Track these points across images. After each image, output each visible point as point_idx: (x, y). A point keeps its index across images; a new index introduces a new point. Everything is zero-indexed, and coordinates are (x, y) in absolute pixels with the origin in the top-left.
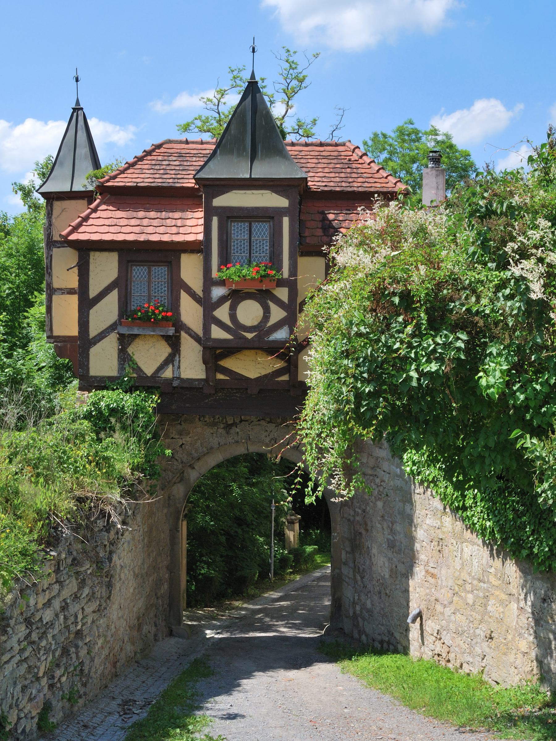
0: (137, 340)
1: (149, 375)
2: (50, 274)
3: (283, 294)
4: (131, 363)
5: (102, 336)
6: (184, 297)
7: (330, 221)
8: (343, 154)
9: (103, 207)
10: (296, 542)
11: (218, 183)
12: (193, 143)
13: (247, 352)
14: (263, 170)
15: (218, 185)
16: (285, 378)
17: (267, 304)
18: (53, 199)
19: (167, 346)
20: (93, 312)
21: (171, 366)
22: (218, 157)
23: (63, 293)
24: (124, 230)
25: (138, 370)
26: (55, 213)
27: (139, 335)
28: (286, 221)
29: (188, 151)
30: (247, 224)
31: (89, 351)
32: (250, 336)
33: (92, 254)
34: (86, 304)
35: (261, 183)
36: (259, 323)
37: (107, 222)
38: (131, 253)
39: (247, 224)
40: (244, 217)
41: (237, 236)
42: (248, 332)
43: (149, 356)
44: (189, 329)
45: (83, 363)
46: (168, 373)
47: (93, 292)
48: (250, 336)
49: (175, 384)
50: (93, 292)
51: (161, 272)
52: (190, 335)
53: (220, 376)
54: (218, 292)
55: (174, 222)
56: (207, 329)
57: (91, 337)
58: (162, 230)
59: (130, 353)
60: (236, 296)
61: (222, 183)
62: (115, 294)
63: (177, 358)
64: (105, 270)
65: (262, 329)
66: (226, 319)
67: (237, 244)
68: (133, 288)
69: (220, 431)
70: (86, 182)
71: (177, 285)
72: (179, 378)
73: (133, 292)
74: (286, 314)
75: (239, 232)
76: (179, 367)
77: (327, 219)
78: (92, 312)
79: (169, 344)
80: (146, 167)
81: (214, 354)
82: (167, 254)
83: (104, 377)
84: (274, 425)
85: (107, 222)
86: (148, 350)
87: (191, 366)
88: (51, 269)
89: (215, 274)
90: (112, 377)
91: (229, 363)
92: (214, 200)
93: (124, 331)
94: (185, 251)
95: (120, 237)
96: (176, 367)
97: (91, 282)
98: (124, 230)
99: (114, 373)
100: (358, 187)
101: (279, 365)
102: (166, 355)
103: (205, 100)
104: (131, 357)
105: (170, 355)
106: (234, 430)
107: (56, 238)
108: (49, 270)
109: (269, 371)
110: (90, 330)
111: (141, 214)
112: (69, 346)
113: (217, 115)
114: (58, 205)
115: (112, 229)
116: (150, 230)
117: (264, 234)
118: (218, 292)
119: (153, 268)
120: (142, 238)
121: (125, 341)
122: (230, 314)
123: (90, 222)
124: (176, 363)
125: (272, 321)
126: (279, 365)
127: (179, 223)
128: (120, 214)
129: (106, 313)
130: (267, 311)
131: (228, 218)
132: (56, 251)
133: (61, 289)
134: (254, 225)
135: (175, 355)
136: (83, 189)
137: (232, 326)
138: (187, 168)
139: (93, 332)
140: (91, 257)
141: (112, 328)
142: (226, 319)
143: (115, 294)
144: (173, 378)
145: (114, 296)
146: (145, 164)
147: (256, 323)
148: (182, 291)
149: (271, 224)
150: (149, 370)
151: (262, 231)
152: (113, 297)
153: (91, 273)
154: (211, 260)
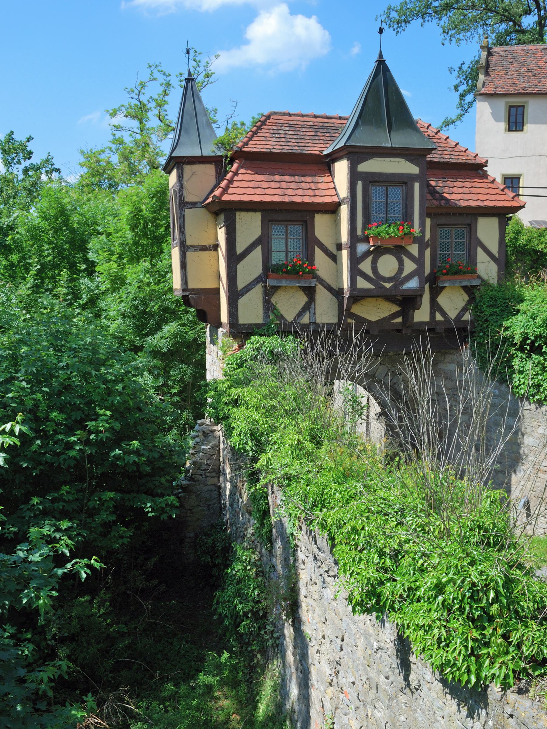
3: (414, 249)
4: (275, 311)
5: (248, 288)
6: (318, 253)
7: (434, 187)
9: (242, 171)
11: (363, 150)
12: (295, 115)
13: (370, 299)
15: (356, 153)
16: (400, 320)
17: (402, 258)
18: (184, 163)
21: (308, 313)
22: (361, 128)
23: (195, 250)
25: (281, 317)
26: (186, 176)
27: (281, 286)
28: (417, 185)
30: (384, 188)
31: (237, 301)
32: (388, 285)
33: (238, 214)
37: (252, 184)
38: (272, 213)
42: (387, 282)
44: (322, 280)
46: (306, 319)
47: (240, 249)
48: (388, 285)
50: (240, 249)
51: (296, 229)
52: (323, 286)
54: (362, 248)
55: (308, 186)
57: (239, 289)
59: (274, 302)
60: (379, 251)
61: (367, 150)
62: (259, 249)
63: (313, 306)
64: (250, 227)
66: (368, 271)
70: (213, 148)
71: (474, 243)
72: (314, 323)
75: (377, 194)
76: (315, 314)
77: (431, 186)
78: (239, 266)
82: (301, 215)
83: (251, 325)
85: (252, 184)
86: (288, 300)
88: (184, 227)
89: (359, 232)
90: (259, 324)
91: (357, 309)
93: (272, 282)
94: (318, 212)
96: (312, 313)
97: (238, 239)
99: (260, 321)
101: (395, 308)
102: (304, 303)
103: (128, 90)
104: (275, 307)
105: (306, 303)
107: (189, 198)
108: (183, 229)
109: (387, 314)
110: (238, 283)
111: (277, 178)
112: (203, 297)
113: (139, 103)
114: (188, 169)
116: (290, 192)
118: (362, 248)
119: (289, 227)
120: (287, 199)
121: (269, 293)
122: (372, 267)
123: (235, 184)
124: (312, 310)
125: (406, 273)
126: (395, 308)
127: (313, 186)
128: (261, 177)
131: (370, 182)
132: (188, 212)
133: (193, 246)
135: (311, 304)
136: (213, 155)
141: (257, 281)
143: (259, 249)
145: (258, 252)
147: (392, 275)
150: (290, 317)
151: (396, 194)
154: (356, 220)
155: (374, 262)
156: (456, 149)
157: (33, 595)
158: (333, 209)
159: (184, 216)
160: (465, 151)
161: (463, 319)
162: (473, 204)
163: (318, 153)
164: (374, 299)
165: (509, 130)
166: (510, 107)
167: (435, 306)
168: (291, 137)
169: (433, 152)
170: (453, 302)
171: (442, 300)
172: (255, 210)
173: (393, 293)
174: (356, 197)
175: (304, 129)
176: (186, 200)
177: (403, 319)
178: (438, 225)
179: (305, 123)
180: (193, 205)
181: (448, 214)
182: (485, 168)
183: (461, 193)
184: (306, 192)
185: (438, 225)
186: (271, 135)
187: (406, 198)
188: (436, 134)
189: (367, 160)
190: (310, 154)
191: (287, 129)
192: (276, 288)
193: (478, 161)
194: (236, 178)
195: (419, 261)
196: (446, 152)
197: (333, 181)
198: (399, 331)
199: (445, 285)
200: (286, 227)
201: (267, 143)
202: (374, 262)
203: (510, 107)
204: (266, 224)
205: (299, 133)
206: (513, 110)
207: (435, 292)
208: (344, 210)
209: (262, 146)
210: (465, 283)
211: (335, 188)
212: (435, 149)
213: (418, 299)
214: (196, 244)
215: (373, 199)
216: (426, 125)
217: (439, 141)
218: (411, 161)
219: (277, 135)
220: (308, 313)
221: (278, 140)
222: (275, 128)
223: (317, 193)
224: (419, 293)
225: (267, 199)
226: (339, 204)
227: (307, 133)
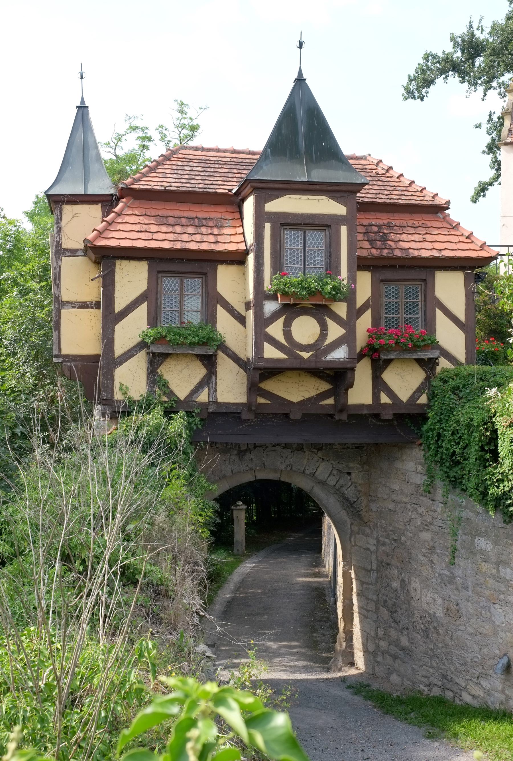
0: (168, 360)
1: (182, 399)
2: (58, 286)
3: (341, 309)
6: (221, 313)
8: (367, 167)
11: (272, 185)
12: (209, 150)
13: (289, 374)
14: (320, 174)
16: (330, 401)
17: (325, 320)
18: (64, 202)
19: (202, 367)
20: (119, 328)
21: (206, 390)
23: (74, 307)
24: (155, 236)
27: (170, 354)
28: (344, 229)
29: (207, 158)
31: (113, 372)
32: (306, 355)
33: (118, 263)
34: (111, 318)
35: (318, 187)
36: (316, 341)
38: (162, 262)
39: (301, 233)
40: (299, 225)
41: (290, 245)
43: (182, 378)
45: (107, 386)
46: (203, 397)
47: (119, 306)
48: (306, 355)
50: (119, 306)
51: (194, 284)
53: (261, 400)
56: (258, 348)
57: (116, 356)
58: (198, 238)
61: (276, 186)
64: (132, 280)
65: (318, 347)
66: (280, 337)
67: (290, 254)
68: (163, 302)
69: (233, 457)
71: (212, 300)
72: (215, 402)
73: (163, 306)
74: (345, 331)
75: (292, 240)
76: (215, 391)
79: (204, 364)
80: (168, 171)
81: (261, 373)
82: (202, 264)
84: (290, 450)
85: (137, 228)
86: (181, 371)
87: (231, 388)
88: (60, 279)
89: (267, 286)
91: (271, 386)
92: (266, 205)
97: (117, 294)
98: (155, 236)
100: (398, 199)
101: (325, 386)
106: (248, 456)
107: (66, 245)
108: (58, 282)
109: (313, 393)
114: (68, 210)
115: (142, 236)
116: (185, 237)
117: (319, 243)
118: (270, 307)
119: (185, 280)
120: (179, 246)
121: (156, 361)
124: (212, 386)
130: (324, 327)
131: (282, 225)
132: (66, 261)
134: (309, 234)
135: (210, 378)
137: (286, 344)
138: (177, 180)
139: (119, 350)
140: (117, 267)
141: (142, 345)
142: (280, 337)
144: (209, 402)
145: (143, 310)
146: (166, 169)
147: (312, 341)
148: (218, 306)
149: (328, 233)
150: (404, 396)
151: (317, 240)
152: (142, 312)
153: (117, 285)
156: (410, 189)
158: (238, 259)
159: (60, 267)
160: (421, 191)
161: (418, 402)
162: (425, 254)
163: (227, 191)
164: (295, 372)
167: (378, 384)
168: (197, 173)
169: (366, 187)
170: (404, 382)
171: (390, 377)
172: (139, 259)
173: (313, 365)
174: (263, 243)
175: (217, 166)
176: (64, 246)
177: (335, 401)
178: (382, 281)
179: (220, 159)
180: (73, 253)
181: (393, 267)
182: (447, 212)
183: (416, 242)
184: (205, 238)
185: (382, 281)
186: (172, 172)
187: (330, 245)
188: (387, 171)
189: (278, 197)
190: (216, 192)
191: (195, 165)
192: (165, 356)
193: (437, 202)
194: (119, 220)
195: (349, 325)
196: (395, 192)
197: (242, 226)
198: (331, 416)
199: (391, 357)
200: (182, 281)
201: (165, 180)
202: (287, 325)
204: (155, 276)
205: (209, 170)
207: (379, 366)
208: (251, 259)
209: (156, 184)
211: (243, 233)
212: (367, 184)
213: (349, 375)
214: (74, 299)
215: (287, 246)
216: (375, 162)
217: (389, 179)
218: (334, 199)
219: (179, 172)
220: (206, 390)
221: (180, 176)
222: (180, 163)
223: (220, 239)
224: (349, 366)
225: (153, 245)
226: (246, 253)
227: (219, 170)
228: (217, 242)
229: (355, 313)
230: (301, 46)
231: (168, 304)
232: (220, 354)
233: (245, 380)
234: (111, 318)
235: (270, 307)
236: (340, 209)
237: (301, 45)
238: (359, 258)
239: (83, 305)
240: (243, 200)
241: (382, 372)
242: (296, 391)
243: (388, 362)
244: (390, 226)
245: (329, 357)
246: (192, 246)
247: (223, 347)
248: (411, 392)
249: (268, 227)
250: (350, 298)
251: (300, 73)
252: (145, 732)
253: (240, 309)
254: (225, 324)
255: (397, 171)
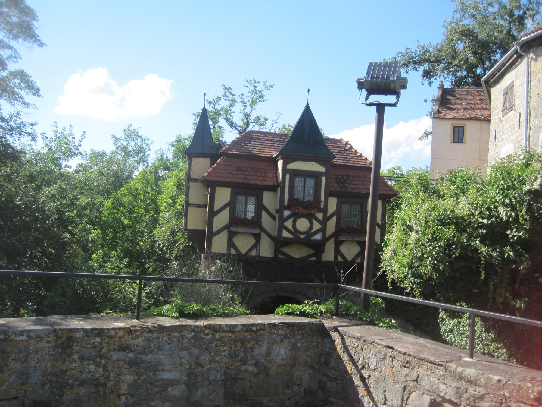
5: (219, 231)
10: (346, 320)
18: (192, 156)
20: (215, 219)
21: (255, 250)
28: (323, 179)
32: (302, 237)
33: (217, 188)
43: (244, 244)
44: (266, 230)
46: (253, 253)
47: (216, 208)
48: (302, 237)
49: (257, 259)
50: (216, 208)
53: (281, 256)
58: (255, 178)
65: (309, 233)
72: (259, 256)
75: (299, 182)
76: (259, 250)
81: (279, 243)
87: (266, 250)
94: (266, 190)
95: (234, 181)
101: (311, 251)
105: (255, 244)
107: (193, 176)
120: (246, 182)
121: (231, 235)
124: (258, 248)
126: (311, 251)
129: (222, 219)
132: (192, 184)
134: (307, 180)
139: (215, 229)
140: (217, 189)
145: (227, 211)
147: (305, 230)
150: (243, 251)
151: (310, 182)
155: (294, 222)
157: (9, 304)
165: (454, 142)
166: (455, 127)
167: (338, 252)
170: (349, 251)
171: (343, 249)
172: (227, 186)
176: (192, 177)
180: (196, 180)
192: (236, 233)
195: (324, 224)
199: (343, 239)
202: (294, 222)
203: (455, 127)
204: (234, 196)
206: (457, 129)
207: (338, 244)
210: (356, 239)
220: (255, 250)
228: (264, 180)
229: (327, 218)
230: (308, 91)
231: (240, 207)
232: (263, 233)
233: (274, 246)
234: (213, 214)
235: (287, 213)
236: (322, 169)
237: (309, 91)
238: (330, 192)
239: (199, 206)
240: (278, 160)
241: (339, 246)
242: (297, 253)
243: (343, 242)
244: (348, 175)
245: (313, 238)
246: (253, 182)
247: (262, 229)
248: (353, 257)
249: (322, 206)
250: (325, 210)
251: (308, 104)
252: (247, 314)
253: (273, 212)
254: (265, 218)
255: (355, 147)
